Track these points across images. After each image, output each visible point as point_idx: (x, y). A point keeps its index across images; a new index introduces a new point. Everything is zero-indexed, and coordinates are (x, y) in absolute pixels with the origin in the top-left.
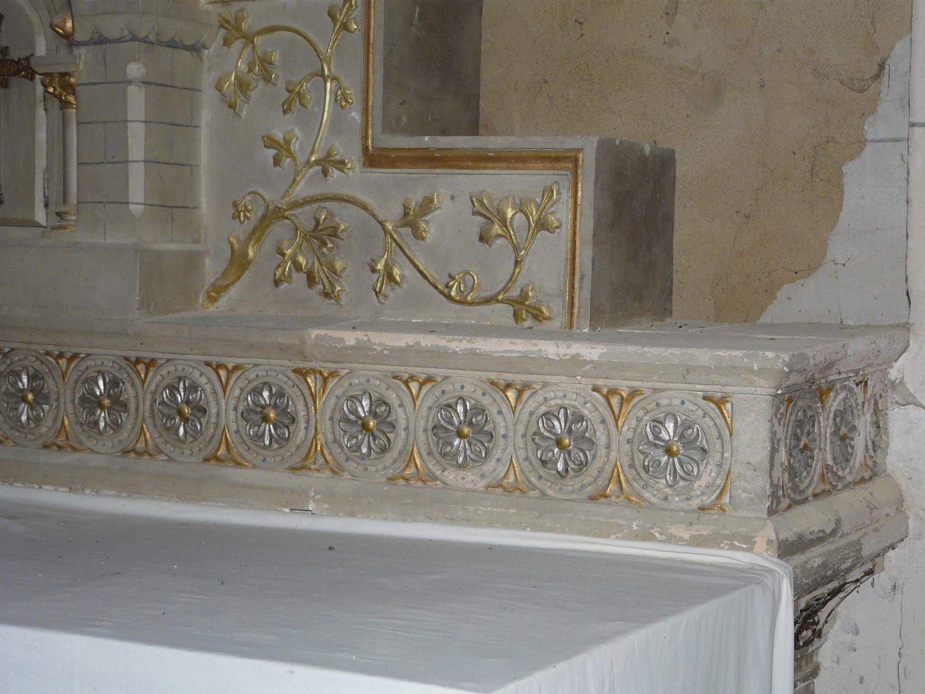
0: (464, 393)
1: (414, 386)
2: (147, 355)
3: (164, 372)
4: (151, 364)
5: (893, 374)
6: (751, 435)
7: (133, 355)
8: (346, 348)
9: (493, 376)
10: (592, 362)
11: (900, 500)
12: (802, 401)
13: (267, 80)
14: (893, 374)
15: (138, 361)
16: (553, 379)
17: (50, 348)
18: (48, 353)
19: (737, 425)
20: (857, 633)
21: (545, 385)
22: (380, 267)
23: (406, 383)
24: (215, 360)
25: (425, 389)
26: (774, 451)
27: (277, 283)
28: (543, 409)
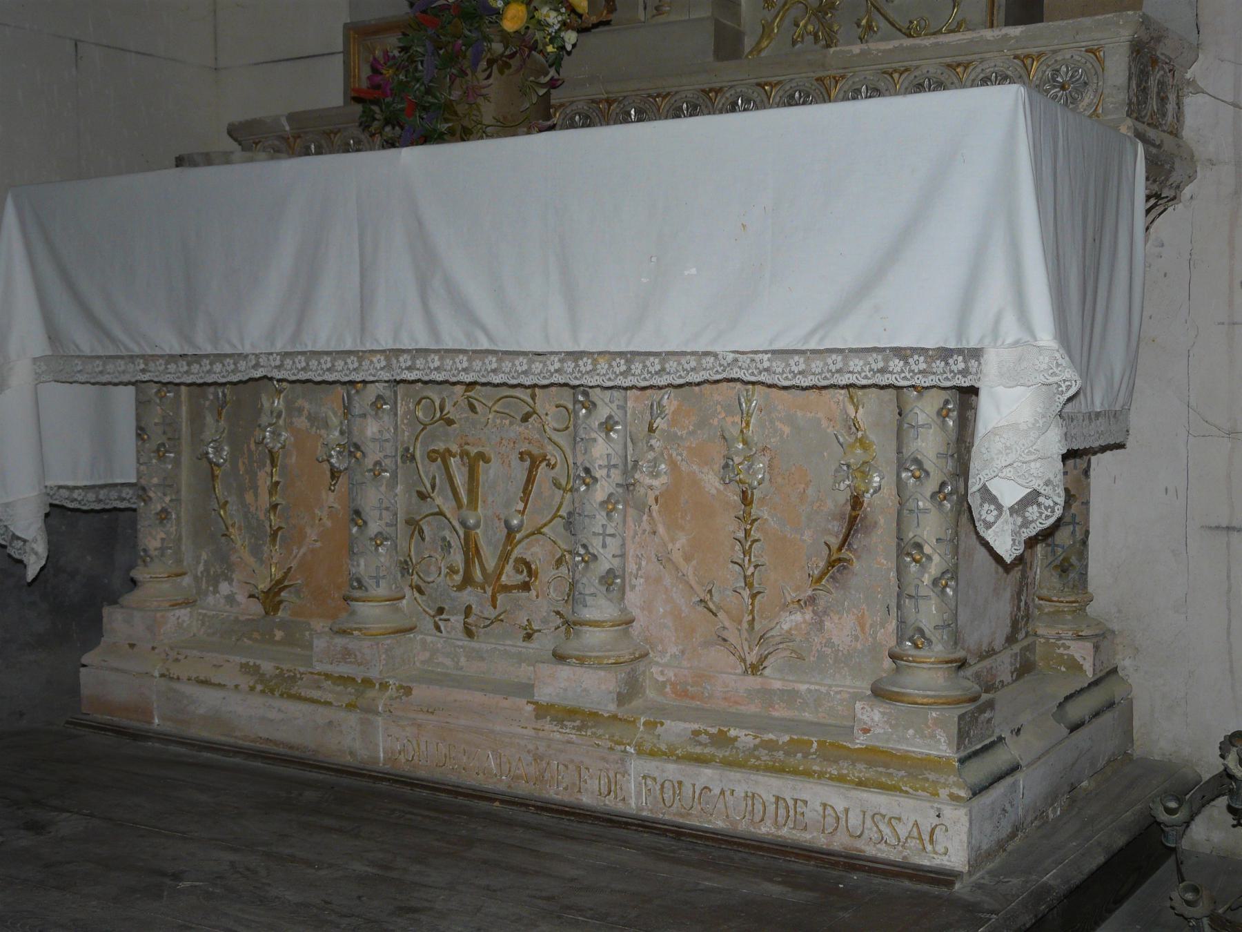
0: (929, 75)
1: (896, 76)
2: (717, 85)
3: (728, 95)
4: (718, 91)
5: (1188, 76)
6: (1117, 68)
7: (706, 87)
8: (854, 56)
9: (948, 60)
10: (1016, 37)
11: (1193, 156)
12: (1145, 57)
13: (293, 679)
14: (1188, 76)
15: (711, 90)
16: (988, 55)
17: (651, 92)
18: (650, 96)
19: (1107, 64)
20: (1163, 245)
21: (983, 60)
22: (864, 22)
23: (891, 75)
24: (762, 80)
25: (903, 77)
26: (1130, 79)
27: (794, 43)
28: (982, 75)
